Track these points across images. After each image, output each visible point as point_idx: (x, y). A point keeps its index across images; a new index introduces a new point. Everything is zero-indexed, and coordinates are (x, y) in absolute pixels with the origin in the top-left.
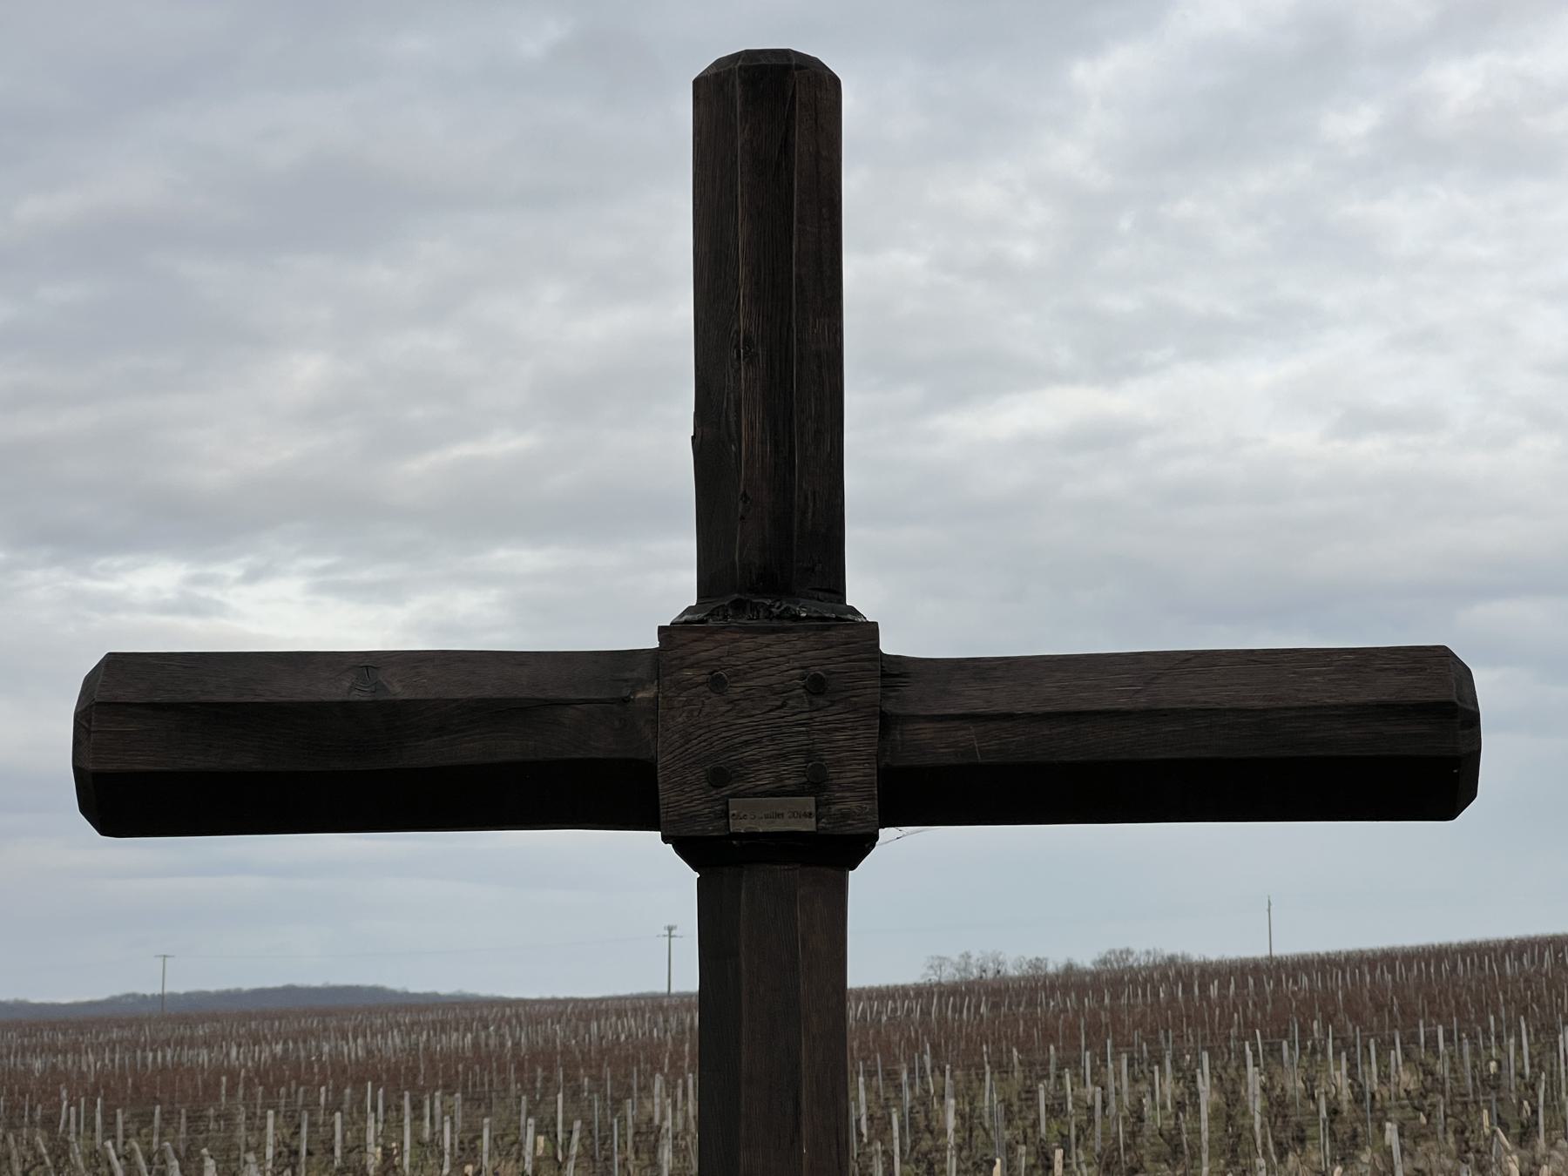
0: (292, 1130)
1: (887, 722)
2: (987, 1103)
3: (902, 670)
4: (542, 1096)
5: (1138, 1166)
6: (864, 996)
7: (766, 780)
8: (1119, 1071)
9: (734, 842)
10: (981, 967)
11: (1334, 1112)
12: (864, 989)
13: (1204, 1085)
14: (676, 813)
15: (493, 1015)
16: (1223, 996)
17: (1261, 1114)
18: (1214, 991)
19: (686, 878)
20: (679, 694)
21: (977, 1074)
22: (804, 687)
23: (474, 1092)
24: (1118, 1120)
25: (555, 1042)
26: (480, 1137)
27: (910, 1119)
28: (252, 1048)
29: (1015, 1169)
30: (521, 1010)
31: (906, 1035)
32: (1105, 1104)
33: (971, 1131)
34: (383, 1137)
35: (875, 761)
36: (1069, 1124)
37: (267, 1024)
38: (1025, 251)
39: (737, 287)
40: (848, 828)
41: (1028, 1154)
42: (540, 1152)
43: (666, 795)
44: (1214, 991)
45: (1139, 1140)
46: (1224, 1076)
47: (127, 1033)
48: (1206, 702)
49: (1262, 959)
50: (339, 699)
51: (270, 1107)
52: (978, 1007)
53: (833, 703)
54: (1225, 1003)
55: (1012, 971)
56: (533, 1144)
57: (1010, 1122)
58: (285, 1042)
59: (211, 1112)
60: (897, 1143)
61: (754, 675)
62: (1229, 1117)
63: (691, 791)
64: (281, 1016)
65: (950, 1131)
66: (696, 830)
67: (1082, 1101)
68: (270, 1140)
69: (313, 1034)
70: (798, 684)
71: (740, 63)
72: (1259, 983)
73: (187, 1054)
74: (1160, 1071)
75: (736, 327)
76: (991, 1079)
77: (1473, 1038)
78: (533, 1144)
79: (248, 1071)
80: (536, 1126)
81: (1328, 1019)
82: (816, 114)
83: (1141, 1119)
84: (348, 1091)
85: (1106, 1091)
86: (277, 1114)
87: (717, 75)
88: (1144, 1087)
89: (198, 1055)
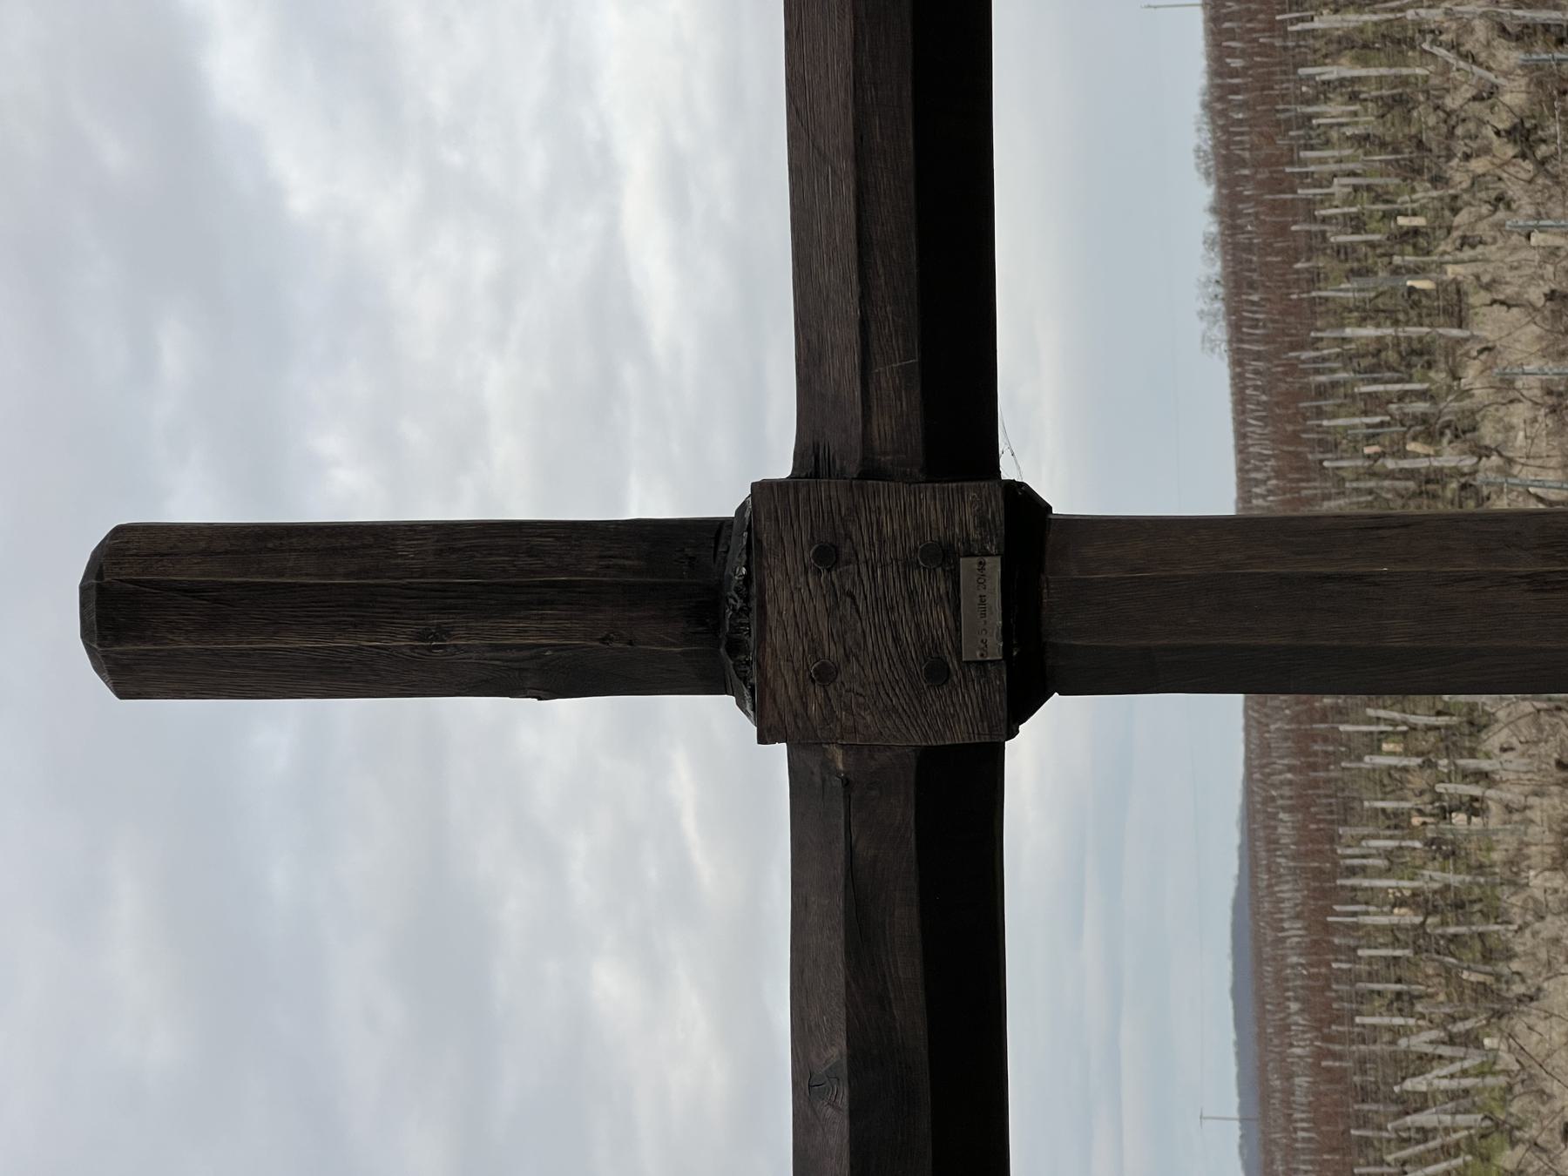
0: (1376, 996)
1: (871, 471)
2: (1350, 295)
3: (810, 452)
4: (1341, 745)
5: (1414, 140)
6: (1242, 418)
7: (939, 617)
8: (1318, 160)
9: (1015, 653)
10: (1212, 300)
12: (1234, 419)
13: (1332, 72)
14: (980, 724)
15: (1260, 792)
16: (1243, 54)
17: (1361, 14)
18: (1237, 63)
20: (838, 719)
21: (1320, 304)
22: (829, 570)
23: (1338, 814)
24: (1367, 161)
25: (1287, 731)
26: (1383, 810)
27: (1366, 372)
28: (1292, 1033)
29: (1419, 267)
30: (1256, 763)
31: (1280, 376)
32: (1353, 174)
33: (1378, 311)
34: (1383, 905)
35: (917, 486)
36: (1372, 212)
37: (1268, 1016)
38: (485, 261)
39: (360, 648)
40: (997, 519)
41: (1402, 254)
42: (1399, 749)
43: (959, 735)
44: (1237, 63)
45: (1388, 139)
46: (1324, 52)
47: (1278, 1156)
48: (846, 90)
49: (1205, 14)
50: (846, 1122)
51: (1352, 1019)
52: (1253, 303)
53: (848, 536)
54: (1250, 51)
55: (1216, 269)
56: (1389, 757)
58: (1288, 999)
59: (1357, 1079)
60: (1390, 387)
61: (815, 630)
62: (1365, 46)
63: (954, 706)
64: (1262, 1003)
65: (1379, 332)
66: (999, 699)
67: (1348, 198)
68: (1385, 1020)
69: (1281, 970)
70: (826, 578)
71: (95, 646)
72: (1229, 17)
73: (1300, 1097)
74: (1318, 118)
75: (408, 652)
76: (1326, 290)
78: (1389, 757)
79: (1316, 1038)
80: (1371, 753)
82: (156, 555)
83: (1367, 137)
84: (1336, 941)
85: (1340, 173)
86: (1360, 1013)
87: (111, 672)
88: (1334, 135)
89: (1300, 1086)
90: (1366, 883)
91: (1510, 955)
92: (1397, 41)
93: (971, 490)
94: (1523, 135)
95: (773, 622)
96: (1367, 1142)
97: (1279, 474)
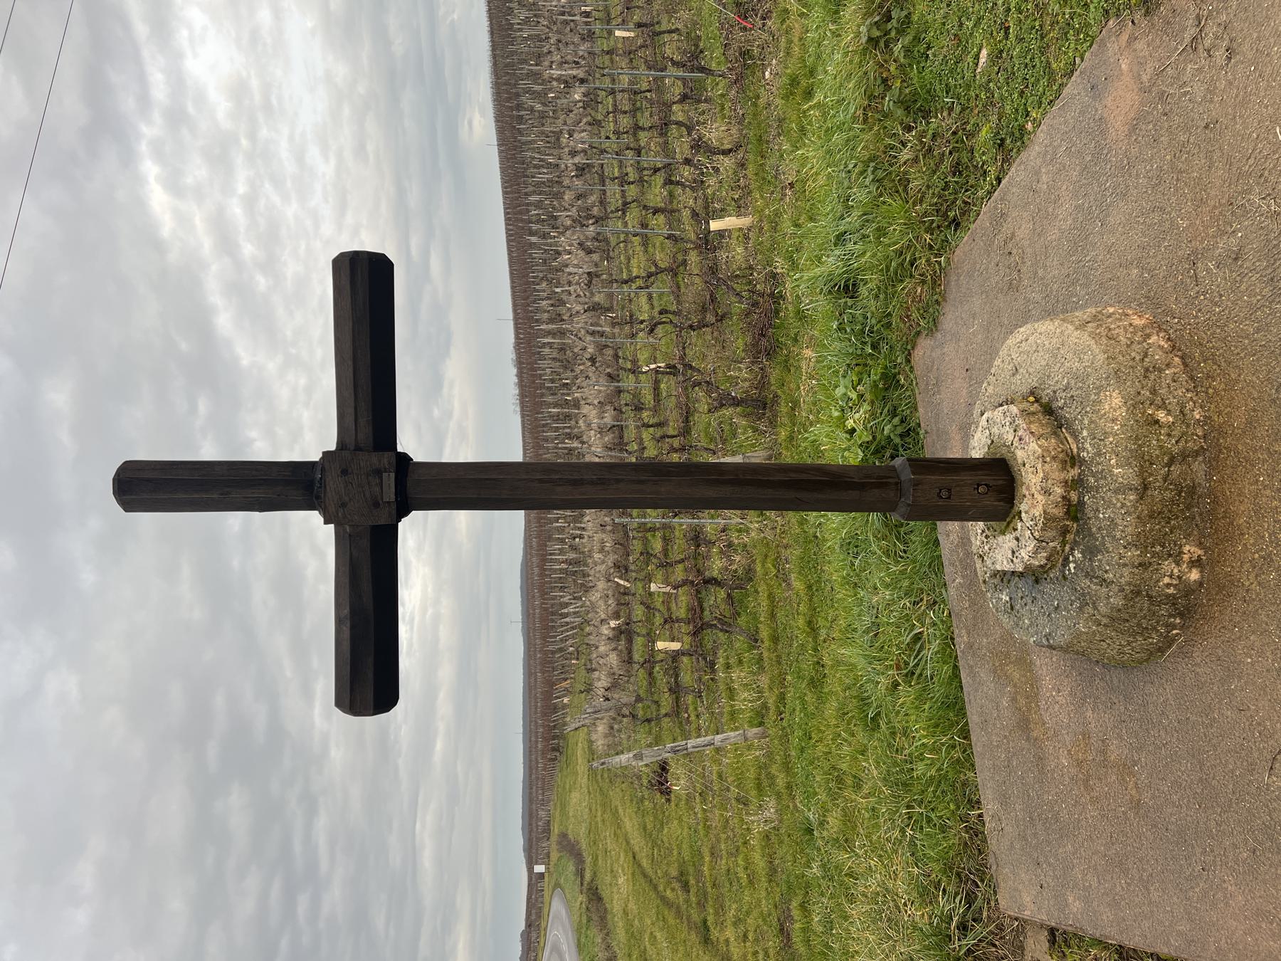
1: (358, 448)
7: (377, 489)
11: (552, 305)
16: (523, 334)
18: (522, 336)
19: (415, 514)
38: (303, 381)
44: (522, 336)
57: (556, 394)
66: (394, 512)
72: (520, 324)
77: (533, 266)
81: (528, 305)
90: (554, 557)
91: (589, 576)
92: (562, 333)
93: (386, 454)
94: (593, 360)
95: (328, 490)
96: (553, 626)
97: (533, 447)
